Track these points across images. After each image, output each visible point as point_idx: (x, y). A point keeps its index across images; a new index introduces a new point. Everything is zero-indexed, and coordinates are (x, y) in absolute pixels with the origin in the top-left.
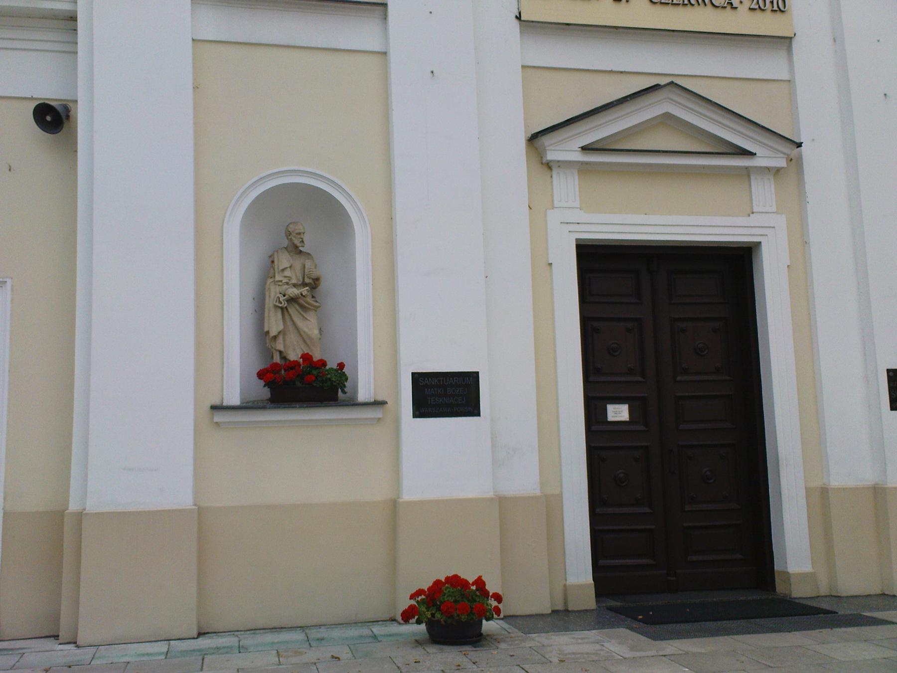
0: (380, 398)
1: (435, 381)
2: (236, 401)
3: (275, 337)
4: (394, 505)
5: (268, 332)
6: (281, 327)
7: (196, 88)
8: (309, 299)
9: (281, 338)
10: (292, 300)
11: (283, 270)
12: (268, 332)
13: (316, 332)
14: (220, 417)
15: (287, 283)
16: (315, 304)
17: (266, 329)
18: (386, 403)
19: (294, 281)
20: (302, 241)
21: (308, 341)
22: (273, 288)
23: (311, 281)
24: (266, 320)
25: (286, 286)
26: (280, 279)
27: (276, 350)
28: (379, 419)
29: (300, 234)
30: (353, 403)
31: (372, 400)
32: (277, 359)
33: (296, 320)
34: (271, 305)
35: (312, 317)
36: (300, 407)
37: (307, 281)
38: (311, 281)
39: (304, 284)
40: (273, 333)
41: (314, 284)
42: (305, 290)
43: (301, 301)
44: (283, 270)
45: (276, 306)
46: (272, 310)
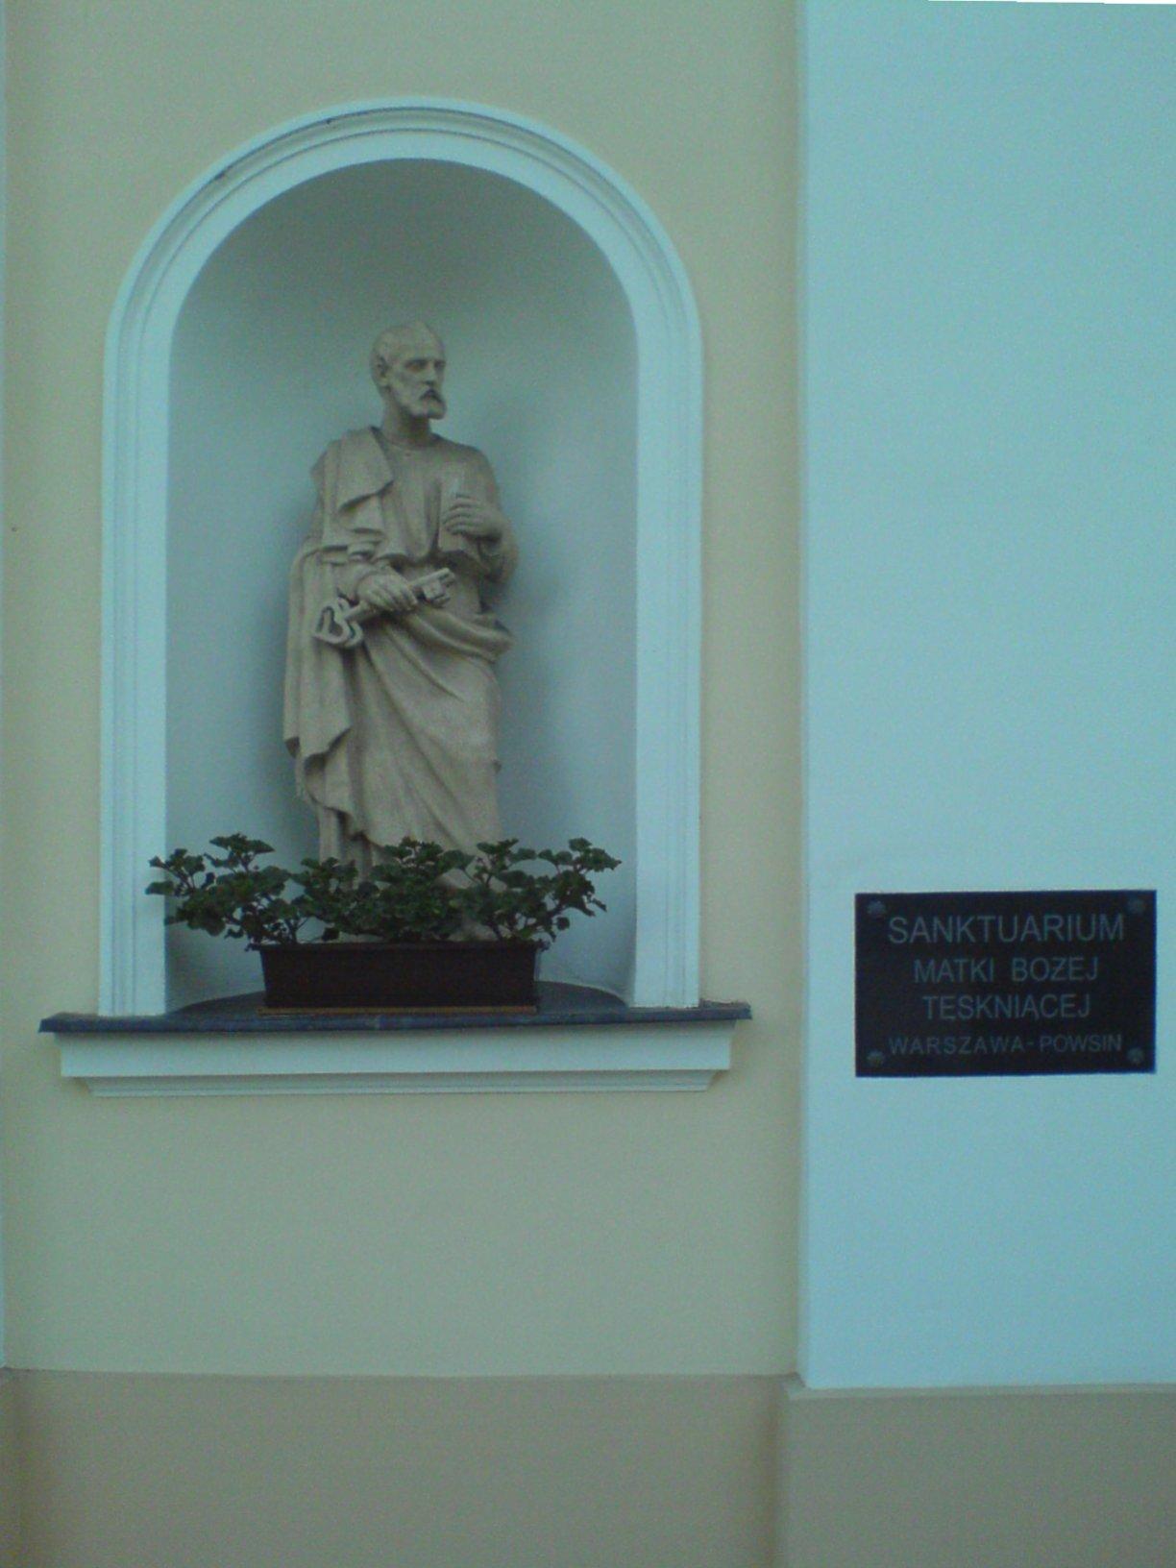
1: (958, 929)
2: (151, 1000)
3: (319, 762)
4: (774, 1395)
5: (294, 745)
6: (339, 723)
7: (328, 121)
9: (341, 762)
10: (382, 620)
11: (352, 506)
14: (82, 1060)
15: (367, 556)
16: (489, 634)
17: (288, 735)
19: (394, 547)
20: (433, 395)
22: (450, 617)
24: (289, 702)
25: (361, 568)
26: (337, 541)
27: (327, 809)
28: (718, 1075)
29: (421, 364)
30: (605, 1011)
31: (691, 1001)
32: (329, 845)
33: (401, 696)
34: (306, 641)
37: (448, 544)
39: (435, 559)
40: (308, 750)
41: (484, 565)
42: (431, 581)
43: (417, 621)
44: (352, 506)
45: (319, 645)
46: (308, 653)
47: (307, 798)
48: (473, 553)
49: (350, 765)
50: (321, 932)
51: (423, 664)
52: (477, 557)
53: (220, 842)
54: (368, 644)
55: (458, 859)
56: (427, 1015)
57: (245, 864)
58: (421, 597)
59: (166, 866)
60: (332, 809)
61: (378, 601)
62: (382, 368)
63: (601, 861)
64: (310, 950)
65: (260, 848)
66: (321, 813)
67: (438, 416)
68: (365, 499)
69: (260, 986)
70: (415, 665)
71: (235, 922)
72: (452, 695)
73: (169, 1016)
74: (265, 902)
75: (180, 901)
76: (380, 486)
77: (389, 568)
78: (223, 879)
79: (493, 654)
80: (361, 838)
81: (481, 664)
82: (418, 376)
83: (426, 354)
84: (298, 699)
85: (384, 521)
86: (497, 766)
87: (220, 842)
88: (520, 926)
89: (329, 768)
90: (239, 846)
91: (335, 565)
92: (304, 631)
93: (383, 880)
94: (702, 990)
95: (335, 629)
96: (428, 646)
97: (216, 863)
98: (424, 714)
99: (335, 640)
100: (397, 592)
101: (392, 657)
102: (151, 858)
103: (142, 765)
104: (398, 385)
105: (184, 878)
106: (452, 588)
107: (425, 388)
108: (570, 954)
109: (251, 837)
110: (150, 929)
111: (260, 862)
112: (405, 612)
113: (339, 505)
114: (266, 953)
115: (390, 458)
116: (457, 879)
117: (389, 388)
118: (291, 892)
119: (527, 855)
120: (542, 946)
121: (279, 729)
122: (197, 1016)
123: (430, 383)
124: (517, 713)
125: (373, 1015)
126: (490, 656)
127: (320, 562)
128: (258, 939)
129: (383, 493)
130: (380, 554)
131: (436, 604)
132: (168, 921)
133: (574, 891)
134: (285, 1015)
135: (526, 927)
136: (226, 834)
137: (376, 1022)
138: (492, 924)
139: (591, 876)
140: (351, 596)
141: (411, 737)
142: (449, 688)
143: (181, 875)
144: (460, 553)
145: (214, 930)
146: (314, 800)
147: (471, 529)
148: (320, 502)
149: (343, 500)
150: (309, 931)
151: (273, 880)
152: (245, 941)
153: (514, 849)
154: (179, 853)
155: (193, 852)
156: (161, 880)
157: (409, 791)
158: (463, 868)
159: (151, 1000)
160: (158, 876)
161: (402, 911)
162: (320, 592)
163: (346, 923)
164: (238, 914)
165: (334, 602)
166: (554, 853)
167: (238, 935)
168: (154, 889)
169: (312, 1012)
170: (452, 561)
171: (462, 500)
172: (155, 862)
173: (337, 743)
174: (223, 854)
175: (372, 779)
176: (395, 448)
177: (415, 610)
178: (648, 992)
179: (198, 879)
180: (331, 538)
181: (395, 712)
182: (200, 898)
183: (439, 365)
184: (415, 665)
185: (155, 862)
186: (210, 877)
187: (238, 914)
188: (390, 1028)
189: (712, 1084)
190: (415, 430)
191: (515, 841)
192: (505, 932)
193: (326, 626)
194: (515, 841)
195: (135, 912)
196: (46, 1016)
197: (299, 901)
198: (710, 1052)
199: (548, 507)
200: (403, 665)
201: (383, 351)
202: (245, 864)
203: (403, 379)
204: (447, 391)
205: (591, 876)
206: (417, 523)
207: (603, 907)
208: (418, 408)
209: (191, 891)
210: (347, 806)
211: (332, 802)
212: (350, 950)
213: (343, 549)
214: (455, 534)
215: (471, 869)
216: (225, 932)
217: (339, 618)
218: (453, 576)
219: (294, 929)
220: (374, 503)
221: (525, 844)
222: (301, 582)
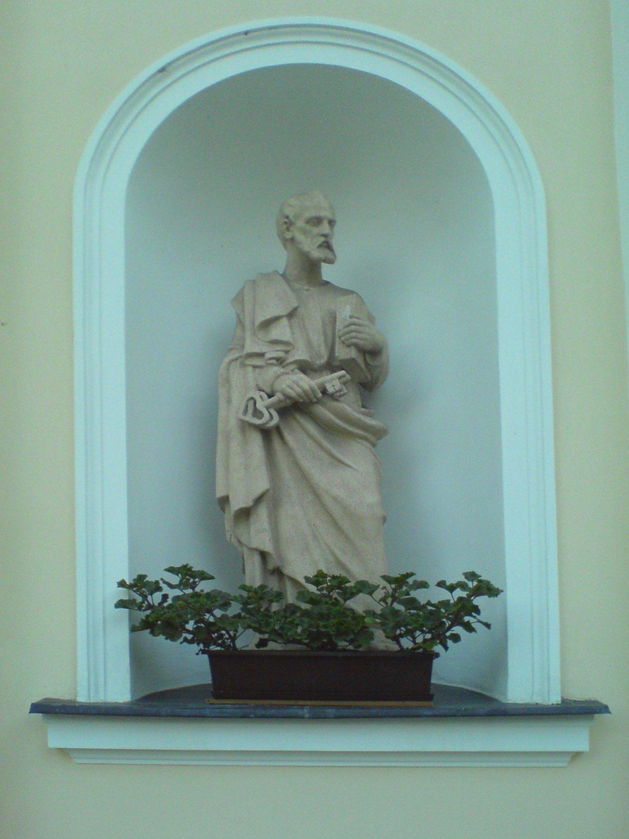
0: (580, 693)
2: (119, 690)
3: (245, 514)
5: (224, 501)
6: (262, 484)
8: (350, 406)
9: (263, 512)
10: (293, 408)
12: (224, 501)
13: (372, 498)
15: (280, 361)
17: (220, 493)
18: (605, 709)
19: (301, 354)
20: (327, 245)
21: (346, 525)
23: (353, 353)
25: (277, 370)
26: (256, 350)
27: (252, 549)
28: (576, 755)
29: (317, 221)
30: (481, 705)
31: (555, 699)
32: (254, 576)
33: (306, 464)
34: (233, 422)
35: (359, 458)
36: (340, 718)
37: (342, 353)
38: (353, 353)
39: (331, 366)
40: (237, 503)
41: (367, 368)
42: (332, 381)
43: (322, 411)
44: (268, 324)
45: (245, 426)
46: (236, 434)
47: (234, 540)
48: (360, 361)
49: (269, 517)
50: (256, 641)
51: (325, 444)
52: (363, 365)
53: (171, 570)
54: (282, 427)
55: (364, 587)
56: (362, 708)
57: (193, 588)
58: (324, 392)
59: (130, 587)
60: (256, 549)
61: (292, 393)
62: (288, 223)
63: (487, 589)
64: (246, 656)
65: (204, 576)
66: (245, 551)
67: (331, 262)
68: (277, 319)
69: (208, 679)
70: (320, 445)
71: (188, 632)
72: (349, 466)
73: (132, 703)
74: (218, 613)
75: (142, 615)
76: (289, 309)
77: (296, 370)
78: (177, 598)
79: (375, 436)
80: (278, 572)
81: (368, 445)
82: (316, 230)
83: (325, 213)
84: (227, 468)
85: (293, 333)
86: (384, 519)
87: (171, 570)
88: (419, 640)
89: (252, 519)
90: (187, 574)
91: (255, 367)
92: (230, 416)
93: (307, 602)
94: (563, 690)
95: (257, 413)
96: (327, 428)
97: (171, 586)
98: (326, 478)
99: (257, 422)
100: (306, 387)
101: (300, 437)
102: (119, 580)
103: (106, 516)
104: (300, 237)
105: (145, 597)
106: (342, 390)
107: (323, 239)
108: (451, 665)
109: (196, 568)
110: (119, 636)
111: (204, 587)
112: (312, 403)
113: (257, 323)
114: (213, 656)
115: (294, 290)
116: (359, 604)
117: (292, 240)
118: (235, 609)
119: (424, 585)
120: (437, 655)
121: (212, 485)
122: (157, 704)
123: (325, 236)
124: (393, 479)
125: (302, 706)
126: (373, 439)
127: (243, 365)
128: (207, 645)
129: (291, 315)
130: (291, 360)
131: (333, 397)
132: (133, 629)
133: (463, 611)
134: (229, 705)
135: (425, 641)
136: (177, 565)
137: (306, 712)
138: (396, 639)
139: (478, 601)
140: (268, 390)
141: (317, 496)
142: (347, 461)
143: (142, 595)
144: (353, 360)
145: (172, 637)
146: (240, 542)
147: (361, 342)
148: (240, 323)
149: (260, 319)
150: (247, 640)
151: (219, 599)
152: (195, 648)
153: (410, 580)
154: (141, 578)
155: (151, 578)
156: (126, 598)
157: (315, 537)
158: (371, 594)
159: (119, 690)
160: (123, 594)
161: (325, 626)
162: (244, 385)
163: (278, 635)
164: (190, 626)
165: (256, 395)
166: (448, 584)
167: (190, 642)
168: (121, 604)
169: (252, 703)
170: (345, 365)
171: (355, 320)
172: (122, 584)
173: (259, 500)
174: (175, 579)
175: (286, 527)
176: (297, 286)
177: (319, 401)
178: (519, 690)
179: (156, 598)
180: (250, 347)
181: (304, 477)
182: (155, 613)
183: (331, 223)
184: (320, 445)
185: (122, 584)
186: (165, 597)
187: (190, 626)
188: (318, 717)
189: (571, 761)
190: (310, 270)
191: (412, 574)
192: (407, 643)
193: (251, 410)
194: (412, 574)
195: (104, 622)
196: (36, 699)
197: (238, 616)
198: (572, 738)
199: (414, 332)
200: (309, 442)
201: (288, 211)
202: (193, 588)
203: (304, 232)
204: (335, 243)
205: (478, 601)
206: (318, 339)
207: (488, 626)
208: (316, 254)
209: (150, 607)
210: (268, 547)
211: (255, 544)
212: (274, 657)
213: (261, 355)
214: (349, 346)
215: (379, 594)
216: (182, 639)
217: (260, 406)
218: (348, 377)
219: (233, 639)
220: (285, 322)
221: (419, 578)
222: (227, 380)
